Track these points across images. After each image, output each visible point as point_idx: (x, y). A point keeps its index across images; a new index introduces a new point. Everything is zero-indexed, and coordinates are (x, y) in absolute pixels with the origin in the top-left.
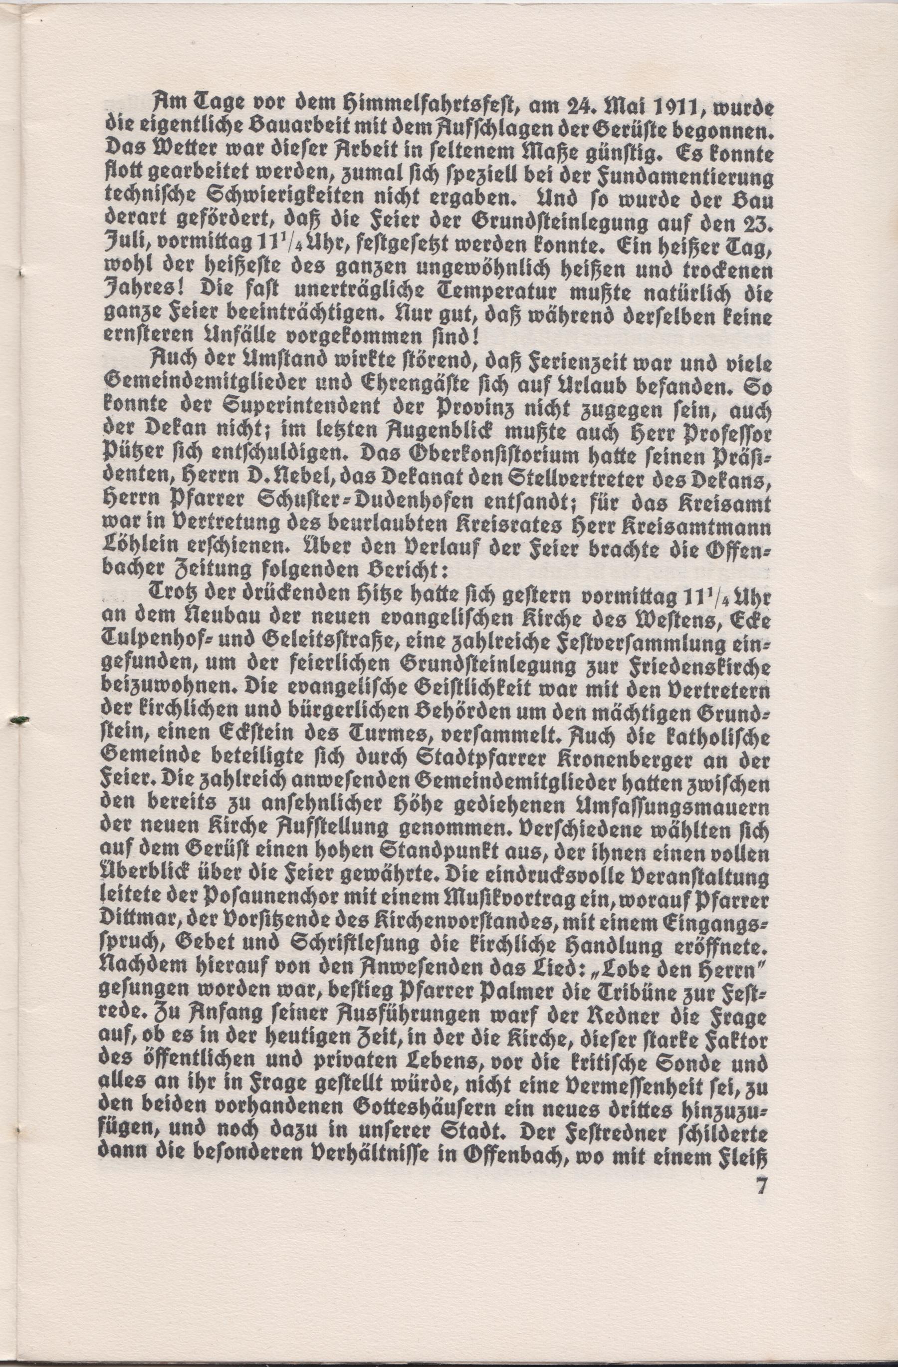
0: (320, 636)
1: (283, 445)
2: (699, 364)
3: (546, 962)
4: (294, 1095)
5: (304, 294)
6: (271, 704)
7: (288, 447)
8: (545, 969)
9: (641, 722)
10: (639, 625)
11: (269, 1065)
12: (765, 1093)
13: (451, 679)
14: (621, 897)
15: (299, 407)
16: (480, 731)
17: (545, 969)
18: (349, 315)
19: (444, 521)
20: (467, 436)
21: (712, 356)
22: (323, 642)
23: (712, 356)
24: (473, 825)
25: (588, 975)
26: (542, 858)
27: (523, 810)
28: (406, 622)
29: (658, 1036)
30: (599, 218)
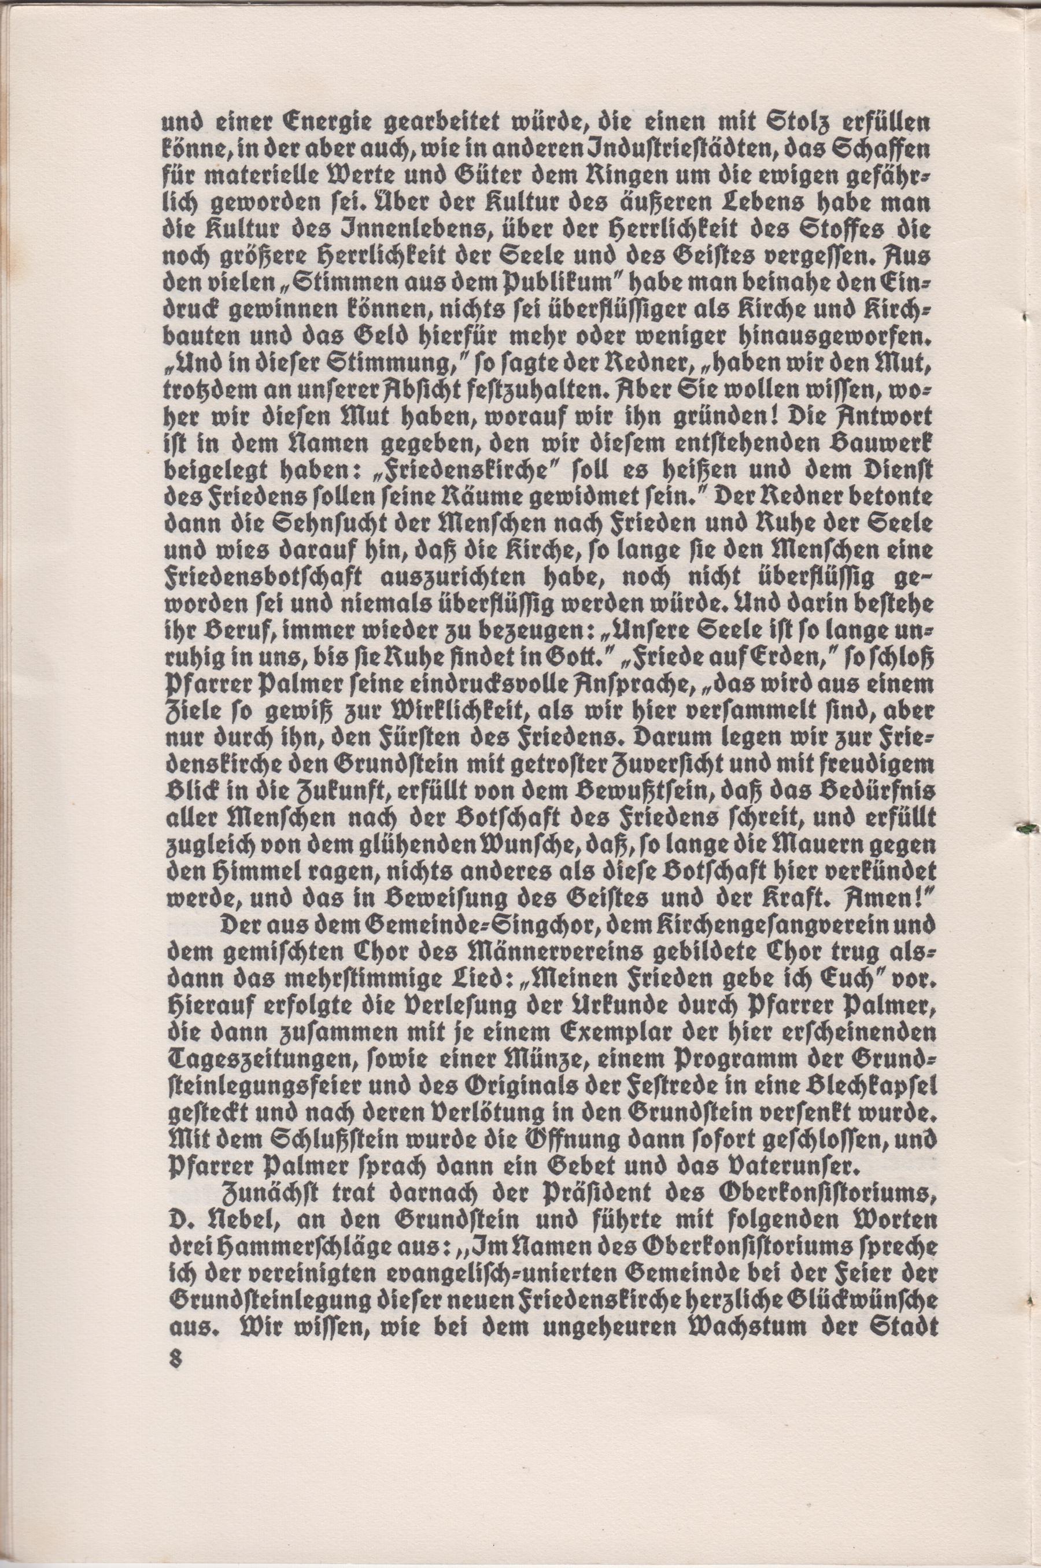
7: (396, 329)
13: (715, 245)
14: (424, 145)
16: (731, 706)
19: (327, 413)
24: (500, 494)
25: (516, 986)
26: (868, 717)
27: (438, 1091)
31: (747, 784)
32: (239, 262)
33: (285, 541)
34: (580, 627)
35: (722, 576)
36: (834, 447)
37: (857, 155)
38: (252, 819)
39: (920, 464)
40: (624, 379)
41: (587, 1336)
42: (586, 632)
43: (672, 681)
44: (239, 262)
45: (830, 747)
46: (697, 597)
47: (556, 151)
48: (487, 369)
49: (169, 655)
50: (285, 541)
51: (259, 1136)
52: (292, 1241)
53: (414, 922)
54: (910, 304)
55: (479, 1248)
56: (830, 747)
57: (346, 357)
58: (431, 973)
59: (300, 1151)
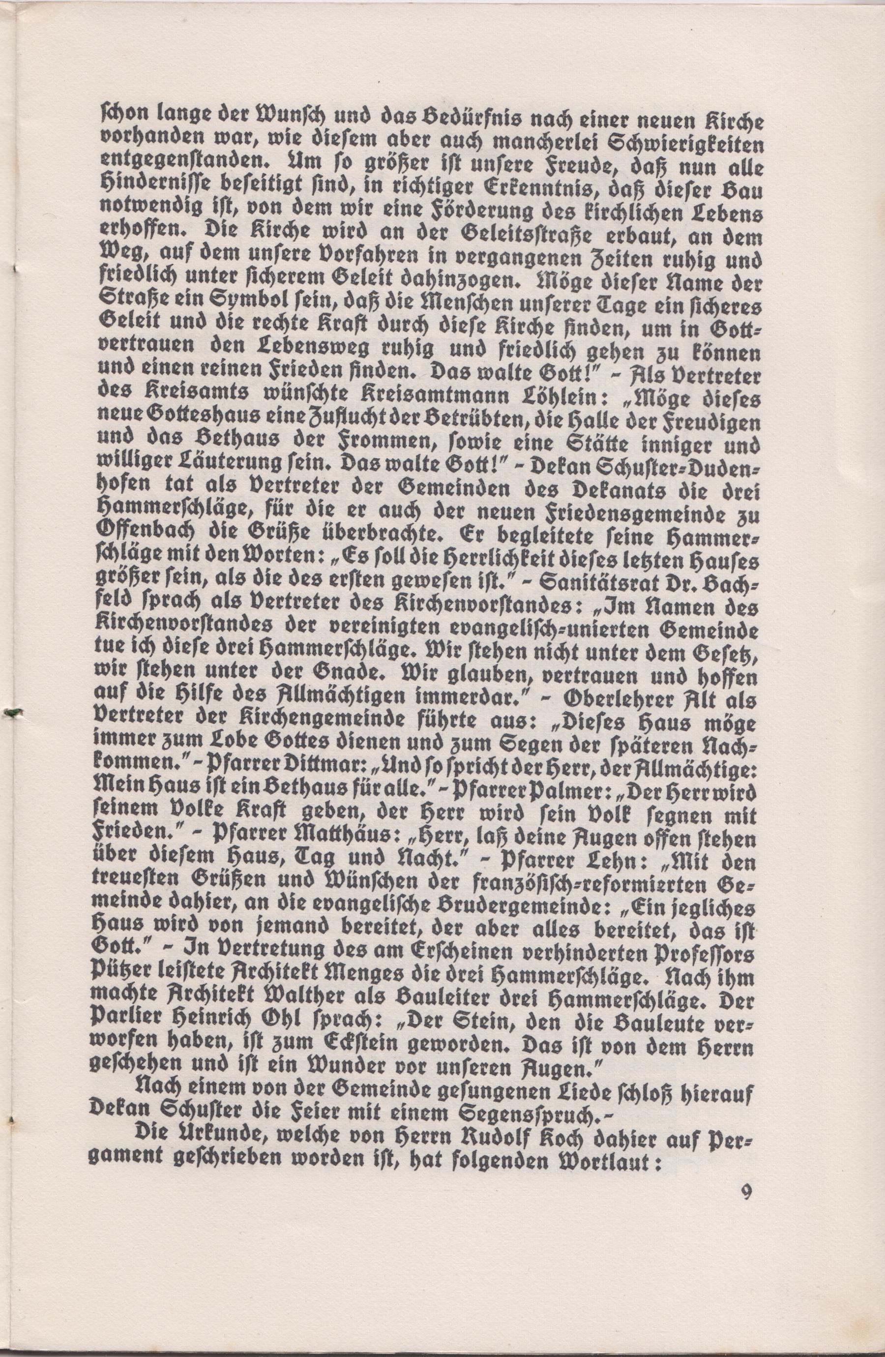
2: (353, 116)
3: (570, 1087)
4: (698, 921)
7: (121, 593)
8: (570, 1093)
9: (139, 1002)
10: (430, 655)
12: (757, 521)
17: (570, 1093)
20: (548, 356)
21: (365, 108)
23: (365, 108)
28: (168, 535)
29: (514, 600)
30: (132, 246)
32: (112, 581)
34: (312, 553)
37: (618, 473)
38: (442, 303)
39: (192, 154)
41: (186, 1164)
42: (317, 557)
44: (112, 581)
49: (385, 345)
52: (162, 501)
53: (133, 735)
54: (741, 581)
55: (190, 949)
58: (747, 719)
59: (201, 1004)
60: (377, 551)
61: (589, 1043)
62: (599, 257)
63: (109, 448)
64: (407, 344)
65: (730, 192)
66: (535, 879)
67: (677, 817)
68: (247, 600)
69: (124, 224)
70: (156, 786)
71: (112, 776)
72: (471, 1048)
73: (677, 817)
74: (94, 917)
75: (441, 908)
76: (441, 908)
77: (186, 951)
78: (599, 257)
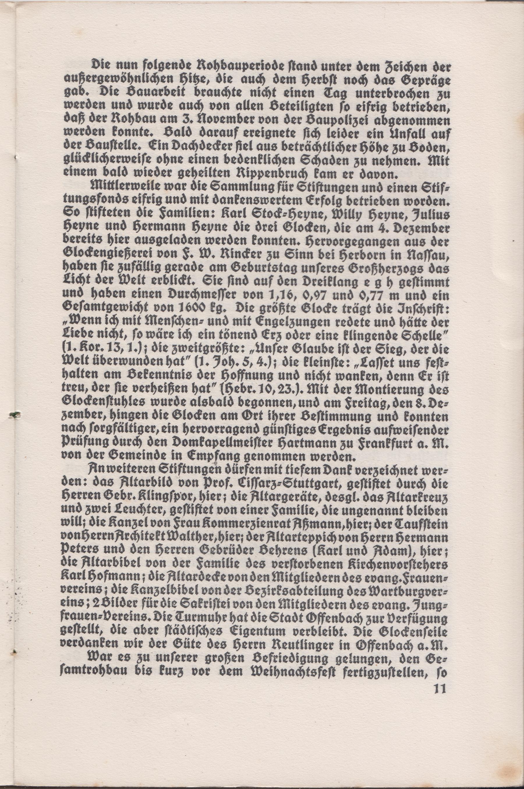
0: (94, 236)
1: (183, 128)
5: (347, 514)
6: (389, 319)
7: (186, 129)
11: (334, 299)
13: (168, 383)
15: (275, 241)
18: (303, 660)
22: (95, 240)
31: (77, 114)
33: (258, 222)
35: (267, 93)
36: (272, 108)
40: (86, 557)
43: (107, 157)
45: (169, 353)
46: (161, 102)
47: (77, 590)
48: (138, 337)
50: (258, 222)
51: (225, 266)
56: (169, 353)
57: (431, 185)
60: (91, 425)
61: (335, 78)
62: (390, 66)
63: (67, 515)
64: (124, 399)
65: (132, 375)
66: (221, 345)
67: (272, 134)
68: (249, 240)
69: (153, 386)
70: (92, 576)
71: (366, 385)
72: (155, 175)
73: (272, 134)
74: (63, 491)
75: (308, 122)
76: (308, 122)
77: (399, 311)
78: (390, 66)
